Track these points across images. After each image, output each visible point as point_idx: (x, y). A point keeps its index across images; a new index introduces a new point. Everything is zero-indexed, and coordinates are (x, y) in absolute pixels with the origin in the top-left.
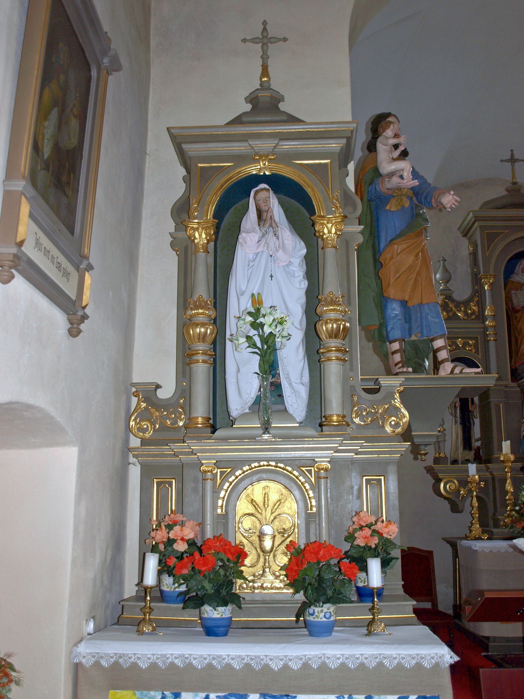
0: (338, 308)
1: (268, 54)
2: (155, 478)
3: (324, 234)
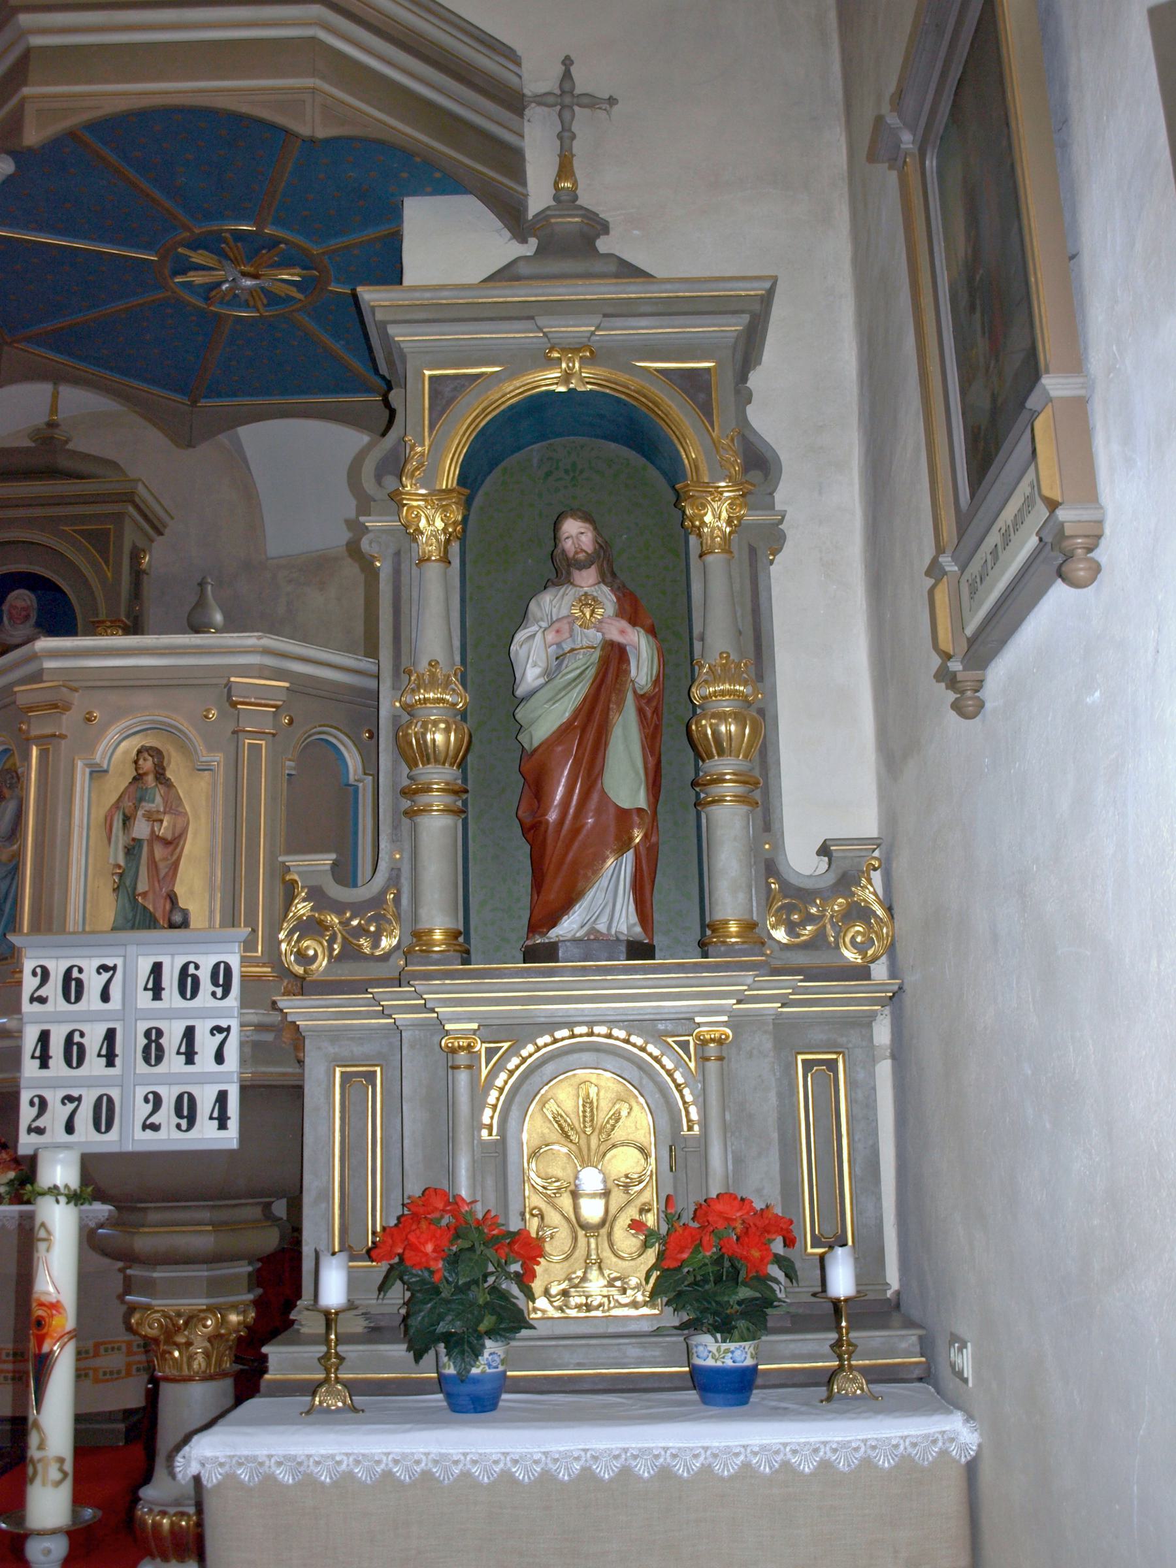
0: (422, 697)
1: (573, 129)
2: (338, 1066)
3: (703, 524)
